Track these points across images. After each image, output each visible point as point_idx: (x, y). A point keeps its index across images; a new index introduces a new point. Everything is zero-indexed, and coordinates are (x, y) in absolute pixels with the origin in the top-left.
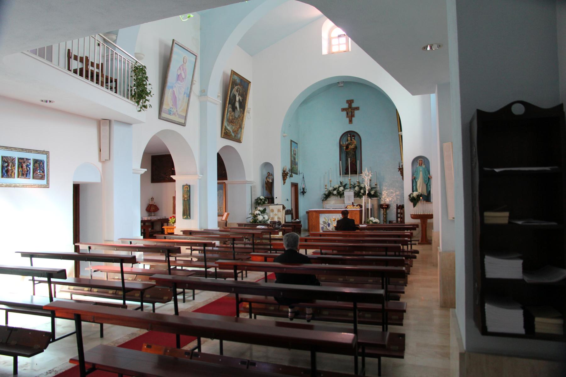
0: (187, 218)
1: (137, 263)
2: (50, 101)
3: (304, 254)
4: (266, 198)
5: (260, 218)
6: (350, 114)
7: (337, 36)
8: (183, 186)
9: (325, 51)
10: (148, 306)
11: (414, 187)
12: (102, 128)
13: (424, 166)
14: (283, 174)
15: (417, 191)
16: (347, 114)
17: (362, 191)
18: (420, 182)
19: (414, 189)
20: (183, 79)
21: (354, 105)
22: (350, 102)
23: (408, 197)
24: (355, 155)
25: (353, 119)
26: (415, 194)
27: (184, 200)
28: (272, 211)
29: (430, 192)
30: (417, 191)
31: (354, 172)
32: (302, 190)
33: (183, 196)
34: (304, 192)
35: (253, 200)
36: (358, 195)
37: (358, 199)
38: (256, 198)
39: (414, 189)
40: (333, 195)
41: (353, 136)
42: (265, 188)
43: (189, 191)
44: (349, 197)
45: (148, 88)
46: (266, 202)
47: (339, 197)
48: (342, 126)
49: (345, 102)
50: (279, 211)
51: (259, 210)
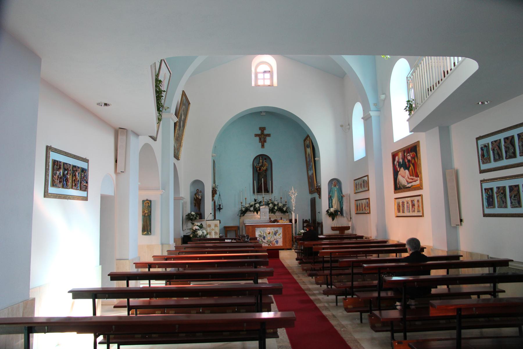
0: (147, 234)
2: (106, 104)
3: (180, 269)
5: (200, 233)
6: (262, 140)
8: (143, 201)
9: (253, 84)
12: (120, 137)
13: (337, 187)
15: (332, 207)
16: (260, 139)
17: (276, 208)
18: (335, 200)
21: (266, 132)
22: (262, 129)
23: (326, 213)
25: (265, 144)
26: (332, 210)
27: (144, 216)
28: (210, 226)
31: (267, 191)
32: (218, 207)
33: (143, 212)
34: (220, 209)
36: (272, 211)
37: (273, 214)
38: (187, 214)
39: (331, 206)
40: (251, 211)
41: (265, 159)
42: (193, 205)
43: (150, 207)
45: (406, 115)
48: (255, 150)
50: (216, 226)
51: (197, 226)
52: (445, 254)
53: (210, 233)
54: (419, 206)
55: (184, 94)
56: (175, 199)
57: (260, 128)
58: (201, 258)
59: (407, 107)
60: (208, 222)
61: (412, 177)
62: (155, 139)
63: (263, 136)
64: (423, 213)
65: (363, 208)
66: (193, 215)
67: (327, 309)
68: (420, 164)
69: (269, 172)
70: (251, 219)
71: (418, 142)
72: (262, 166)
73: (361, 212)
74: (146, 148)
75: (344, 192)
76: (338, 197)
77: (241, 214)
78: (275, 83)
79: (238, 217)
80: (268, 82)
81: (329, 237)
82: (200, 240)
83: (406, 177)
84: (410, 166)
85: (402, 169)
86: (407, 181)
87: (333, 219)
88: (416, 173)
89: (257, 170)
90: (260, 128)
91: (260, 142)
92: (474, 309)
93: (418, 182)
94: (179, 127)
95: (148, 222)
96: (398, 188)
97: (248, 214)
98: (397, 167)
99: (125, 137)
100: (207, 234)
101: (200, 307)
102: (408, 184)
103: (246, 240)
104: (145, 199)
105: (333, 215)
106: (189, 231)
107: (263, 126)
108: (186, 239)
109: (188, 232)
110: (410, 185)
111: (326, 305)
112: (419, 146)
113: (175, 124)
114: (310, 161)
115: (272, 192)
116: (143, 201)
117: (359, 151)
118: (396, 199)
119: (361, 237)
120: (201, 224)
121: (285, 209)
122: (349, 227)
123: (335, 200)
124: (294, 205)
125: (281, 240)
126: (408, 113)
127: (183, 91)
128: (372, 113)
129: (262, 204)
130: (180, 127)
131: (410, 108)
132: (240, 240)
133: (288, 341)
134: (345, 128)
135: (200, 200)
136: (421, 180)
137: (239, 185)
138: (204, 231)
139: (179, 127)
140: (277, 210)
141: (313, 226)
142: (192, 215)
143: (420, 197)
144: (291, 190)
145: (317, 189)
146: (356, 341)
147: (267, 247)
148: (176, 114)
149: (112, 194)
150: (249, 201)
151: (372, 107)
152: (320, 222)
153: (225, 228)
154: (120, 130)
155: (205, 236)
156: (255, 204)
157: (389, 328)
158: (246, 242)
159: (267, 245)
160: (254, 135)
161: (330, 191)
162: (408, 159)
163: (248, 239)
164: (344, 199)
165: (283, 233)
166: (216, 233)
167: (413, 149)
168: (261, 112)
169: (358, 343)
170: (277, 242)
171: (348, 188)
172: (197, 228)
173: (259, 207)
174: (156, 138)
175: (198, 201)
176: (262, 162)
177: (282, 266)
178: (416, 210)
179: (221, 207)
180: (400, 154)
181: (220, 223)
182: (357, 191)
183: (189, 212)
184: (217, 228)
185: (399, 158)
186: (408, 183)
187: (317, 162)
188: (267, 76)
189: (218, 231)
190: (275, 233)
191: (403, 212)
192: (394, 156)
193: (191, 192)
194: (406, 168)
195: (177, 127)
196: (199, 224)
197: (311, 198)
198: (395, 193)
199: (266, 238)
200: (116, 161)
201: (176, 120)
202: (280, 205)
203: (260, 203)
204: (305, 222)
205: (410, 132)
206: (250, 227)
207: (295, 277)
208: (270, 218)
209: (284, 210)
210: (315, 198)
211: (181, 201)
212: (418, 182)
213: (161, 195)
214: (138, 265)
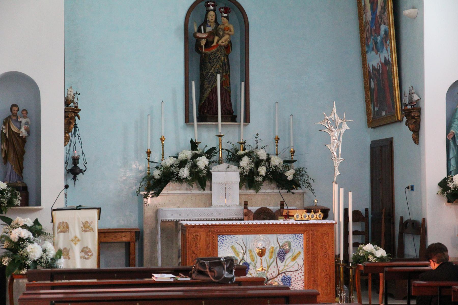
1: (318, 303)
5: (34, 251)
8: (418, 144)
17: (262, 170)
23: (438, 189)
28: (65, 228)
31: (230, 116)
36: (249, 180)
37: (252, 192)
40: (180, 180)
44: (226, 186)
46: (17, 202)
50: (86, 227)
51: (24, 227)
60: (60, 216)
69: (235, 56)
72: (215, 33)
97: (170, 189)
100: (59, 253)
114: (376, 21)
115: (247, 120)
120: (36, 222)
121: (290, 175)
135: (24, 140)
138: (49, 245)
140: (265, 178)
150: (171, 148)
155: (51, 263)
156: (195, 157)
158: (226, 282)
163: (231, 272)
166: (85, 251)
172: (25, 234)
176: (216, 21)
179: (81, 165)
196: (29, 222)
202: (276, 161)
203: (210, 153)
206: (202, 234)
208: (246, 205)
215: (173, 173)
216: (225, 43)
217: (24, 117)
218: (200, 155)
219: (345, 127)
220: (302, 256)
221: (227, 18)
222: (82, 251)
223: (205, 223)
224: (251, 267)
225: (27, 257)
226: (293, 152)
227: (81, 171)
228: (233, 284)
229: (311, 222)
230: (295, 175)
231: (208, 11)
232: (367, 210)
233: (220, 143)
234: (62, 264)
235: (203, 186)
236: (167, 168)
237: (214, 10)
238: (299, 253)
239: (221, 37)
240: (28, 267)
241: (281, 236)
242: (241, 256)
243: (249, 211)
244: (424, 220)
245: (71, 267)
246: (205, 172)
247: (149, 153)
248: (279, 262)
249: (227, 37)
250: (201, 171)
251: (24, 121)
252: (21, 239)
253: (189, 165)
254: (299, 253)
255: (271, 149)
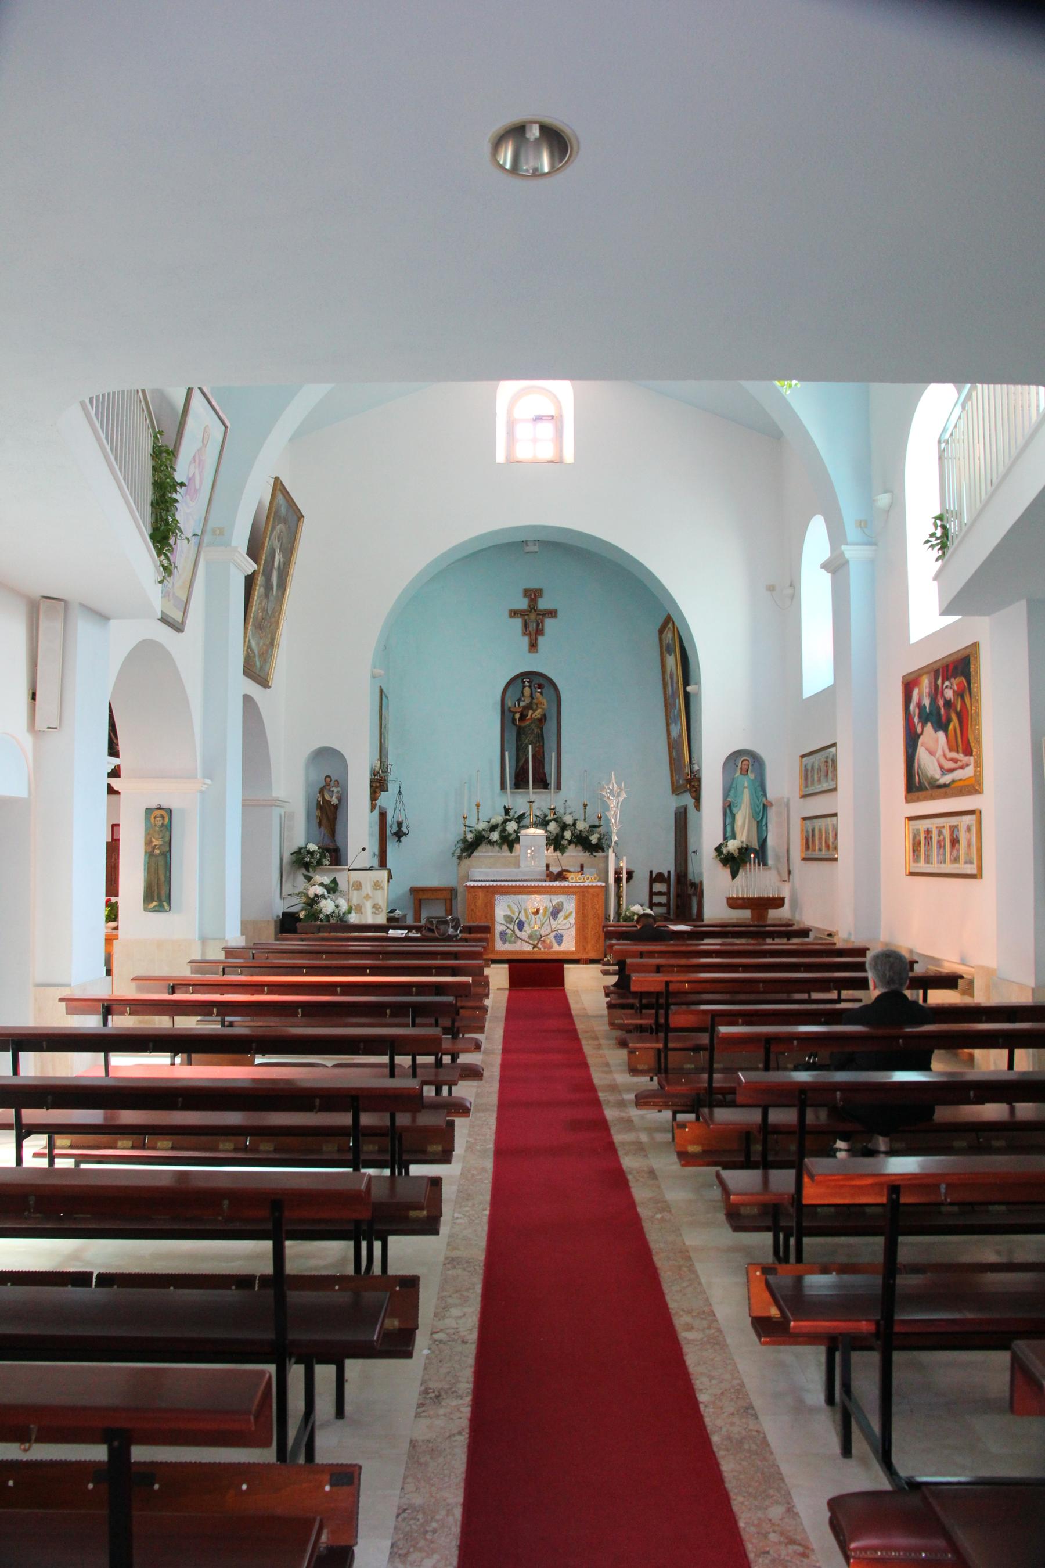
4: (324, 850)
5: (327, 906)
6: (533, 626)
7: (532, 416)
8: (149, 811)
9: (500, 457)
10: (783, 1180)
11: (729, 829)
12: (43, 624)
14: (372, 781)
15: (734, 837)
16: (526, 625)
17: (568, 835)
18: (743, 817)
19: (728, 834)
20: (196, 491)
21: (543, 604)
22: (533, 595)
23: (714, 854)
24: (540, 738)
25: (540, 639)
26: (733, 846)
27: (150, 855)
28: (358, 886)
29: (765, 840)
30: (734, 837)
31: (542, 783)
32: (395, 829)
33: (148, 843)
34: (399, 835)
35: (287, 857)
36: (556, 842)
38: (294, 849)
39: (729, 833)
40: (491, 843)
41: (540, 686)
42: (315, 822)
46: (326, 862)
47: (505, 847)
49: (521, 594)
50: (377, 886)
51: (321, 884)
52: (1023, 998)
53: (359, 909)
54: (969, 845)
55: (278, 486)
56: (247, 805)
57: (527, 593)
58: (275, 988)
59: (933, 535)
60: (355, 876)
61: (954, 755)
62: (178, 627)
63: (533, 616)
64: (980, 868)
65: (820, 846)
66: (312, 853)
67: (640, 1148)
68: (978, 714)
69: (550, 727)
70: (486, 868)
71: (976, 645)
72: (529, 707)
73: (817, 854)
74: (146, 657)
75: (772, 793)
76: (753, 806)
77: (463, 851)
78: (569, 457)
79: (455, 860)
80: (547, 452)
81: (723, 931)
82: (334, 928)
83: (939, 753)
84: (949, 720)
85: (929, 727)
86: (941, 767)
87: (734, 875)
88: (965, 744)
89: (514, 720)
90: (527, 593)
91: (524, 634)
92: (943, 1187)
93: (969, 772)
94: (264, 590)
95: (161, 872)
96: (916, 786)
97: (483, 852)
98: (916, 720)
99: (59, 625)
101: (247, 1135)
102: (943, 774)
103: (451, 931)
104: (154, 805)
105: (734, 862)
106: (295, 900)
107: (536, 586)
108: (288, 923)
109: (296, 905)
110: (947, 779)
111: (644, 1137)
112: (977, 658)
113: (250, 581)
114: (675, 694)
115: (559, 787)
116: (149, 811)
117: (817, 672)
118: (910, 819)
119: (805, 933)
120: (334, 881)
121: (594, 839)
122: (783, 899)
123: (743, 817)
124: (615, 829)
125: (573, 932)
126: (936, 553)
127: (277, 479)
128: (851, 552)
129: (526, 822)
130: (268, 586)
131: (944, 541)
132: (432, 931)
133: (483, 1243)
134: (779, 595)
135: (336, 807)
136: (978, 764)
137: (458, 769)
139: (264, 590)
140: (570, 842)
141: (682, 891)
142: (309, 852)
143: (973, 817)
144: (609, 782)
145: (689, 781)
146: (685, 1255)
147: (529, 953)
148: (253, 552)
149: (23, 793)
151: (852, 532)
152: (697, 881)
153: (415, 891)
154: (44, 605)
157: (769, 1223)
158: (450, 938)
159: (529, 948)
160: (507, 614)
161: (729, 788)
162: (943, 698)
163: (455, 928)
164: (772, 813)
165: (577, 913)
166: (376, 907)
167: (960, 667)
168: (525, 543)
169: (689, 1258)
170: (559, 938)
171: (782, 782)
172: (320, 891)
173: (516, 832)
174: (183, 623)
175: (328, 813)
177: (566, 1013)
178: (962, 858)
179: (404, 829)
180: (926, 682)
181: (390, 877)
182: (810, 790)
183: (302, 844)
184: (379, 892)
185: (922, 694)
186: (945, 771)
187: (692, 699)
188: (546, 429)
189: (382, 902)
190: (555, 913)
191: (928, 860)
192: (909, 686)
193: (308, 784)
194: (941, 725)
195: (258, 590)
196: (326, 880)
197: (677, 808)
198: (907, 801)
199: (526, 927)
200: (34, 696)
201: (251, 567)
202: (581, 826)
203: (520, 819)
204: (657, 878)
205: (945, 612)
207: (588, 1048)
209: (590, 843)
210: (685, 808)
211: (276, 812)
212: (969, 772)
213: (202, 792)
214: (75, 1005)
215: (483, 837)
216: (539, 716)
217: (337, 786)
218: (510, 820)
219: (624, 795)
220: (574, 915)
221: (541, 693)
222: (374, 907)
223: (483, 884)
224: (526, 925)
225: (321, 912)
226: (600, 818)
227: (405, 834)
228: (457, 941)
229: (586, 884)
230: (599, 839)
231: (524, 687)
232: (669, 872)
233: (531, 808)
234: (353, 919)
235: (511, 849)
236: (479, 832)
237: (530, 686)
238: (571, 913)
239: (534, 711)
240: (322, 921)
241: (553, 897)
242: (517, 914)
243: (551, 873)
244: (701, 883)
245: (363, 922)
246: (514, 836)
247: (465, 818)
248: (552, 920)
249: (539, 710)
250: (510, 835)
251: (335, 790)
252: (316, 895)
253: (499, 829)
254: (571, 913)
255: (579, 815)
